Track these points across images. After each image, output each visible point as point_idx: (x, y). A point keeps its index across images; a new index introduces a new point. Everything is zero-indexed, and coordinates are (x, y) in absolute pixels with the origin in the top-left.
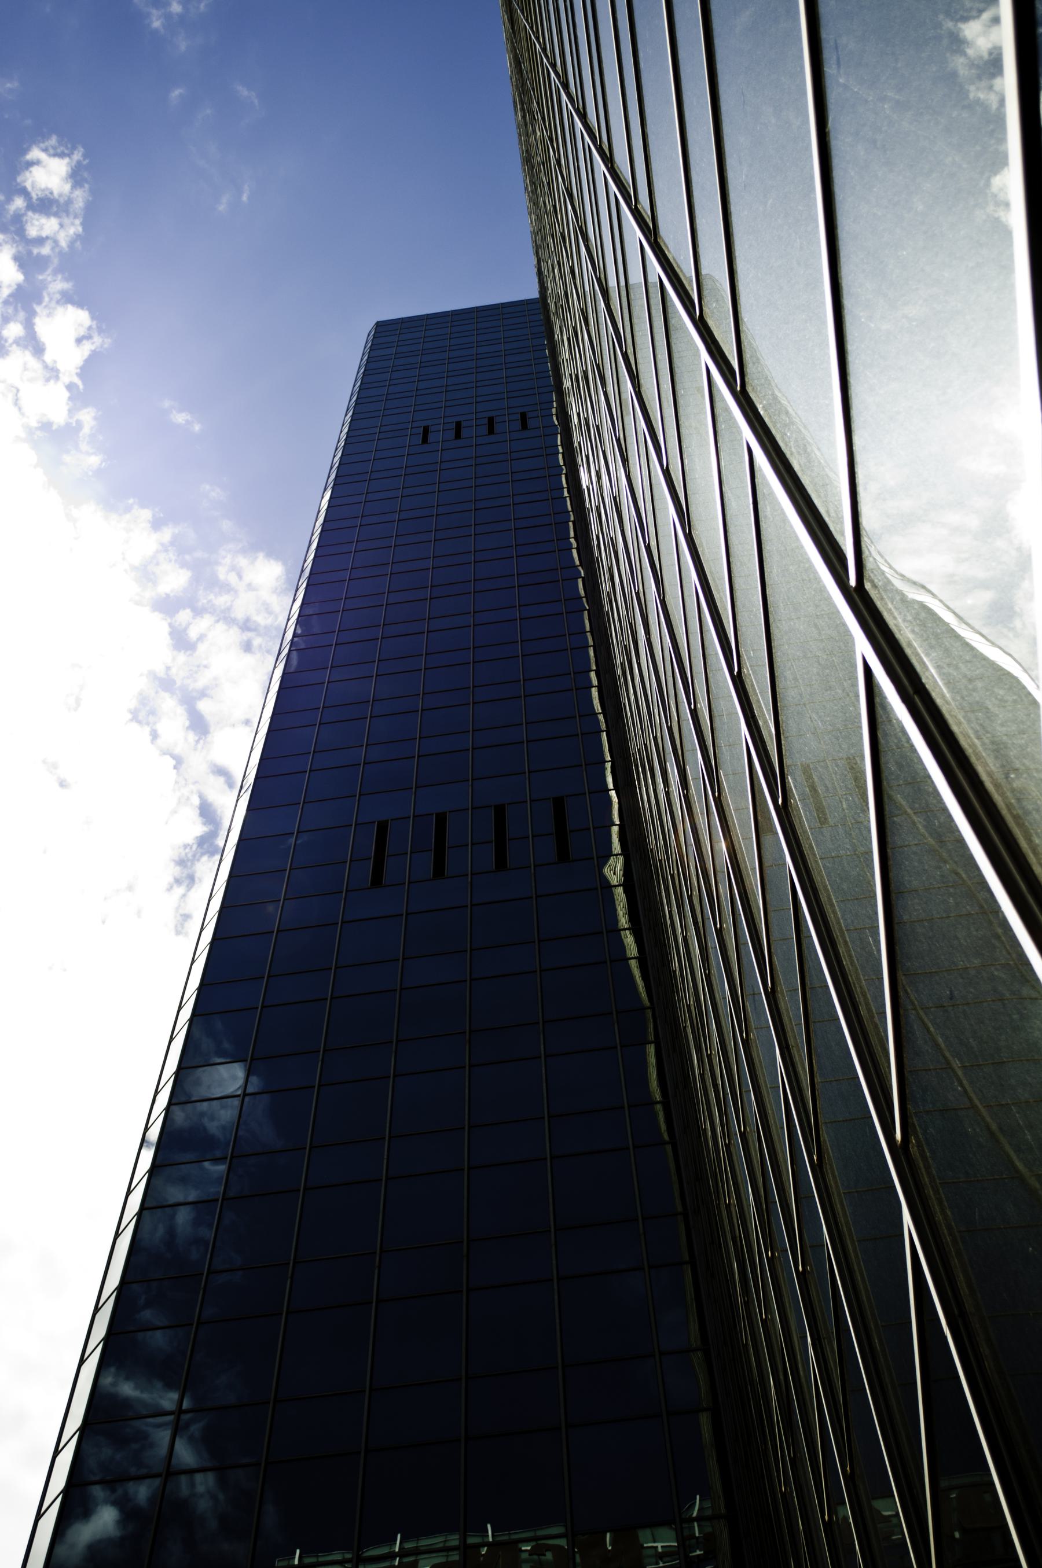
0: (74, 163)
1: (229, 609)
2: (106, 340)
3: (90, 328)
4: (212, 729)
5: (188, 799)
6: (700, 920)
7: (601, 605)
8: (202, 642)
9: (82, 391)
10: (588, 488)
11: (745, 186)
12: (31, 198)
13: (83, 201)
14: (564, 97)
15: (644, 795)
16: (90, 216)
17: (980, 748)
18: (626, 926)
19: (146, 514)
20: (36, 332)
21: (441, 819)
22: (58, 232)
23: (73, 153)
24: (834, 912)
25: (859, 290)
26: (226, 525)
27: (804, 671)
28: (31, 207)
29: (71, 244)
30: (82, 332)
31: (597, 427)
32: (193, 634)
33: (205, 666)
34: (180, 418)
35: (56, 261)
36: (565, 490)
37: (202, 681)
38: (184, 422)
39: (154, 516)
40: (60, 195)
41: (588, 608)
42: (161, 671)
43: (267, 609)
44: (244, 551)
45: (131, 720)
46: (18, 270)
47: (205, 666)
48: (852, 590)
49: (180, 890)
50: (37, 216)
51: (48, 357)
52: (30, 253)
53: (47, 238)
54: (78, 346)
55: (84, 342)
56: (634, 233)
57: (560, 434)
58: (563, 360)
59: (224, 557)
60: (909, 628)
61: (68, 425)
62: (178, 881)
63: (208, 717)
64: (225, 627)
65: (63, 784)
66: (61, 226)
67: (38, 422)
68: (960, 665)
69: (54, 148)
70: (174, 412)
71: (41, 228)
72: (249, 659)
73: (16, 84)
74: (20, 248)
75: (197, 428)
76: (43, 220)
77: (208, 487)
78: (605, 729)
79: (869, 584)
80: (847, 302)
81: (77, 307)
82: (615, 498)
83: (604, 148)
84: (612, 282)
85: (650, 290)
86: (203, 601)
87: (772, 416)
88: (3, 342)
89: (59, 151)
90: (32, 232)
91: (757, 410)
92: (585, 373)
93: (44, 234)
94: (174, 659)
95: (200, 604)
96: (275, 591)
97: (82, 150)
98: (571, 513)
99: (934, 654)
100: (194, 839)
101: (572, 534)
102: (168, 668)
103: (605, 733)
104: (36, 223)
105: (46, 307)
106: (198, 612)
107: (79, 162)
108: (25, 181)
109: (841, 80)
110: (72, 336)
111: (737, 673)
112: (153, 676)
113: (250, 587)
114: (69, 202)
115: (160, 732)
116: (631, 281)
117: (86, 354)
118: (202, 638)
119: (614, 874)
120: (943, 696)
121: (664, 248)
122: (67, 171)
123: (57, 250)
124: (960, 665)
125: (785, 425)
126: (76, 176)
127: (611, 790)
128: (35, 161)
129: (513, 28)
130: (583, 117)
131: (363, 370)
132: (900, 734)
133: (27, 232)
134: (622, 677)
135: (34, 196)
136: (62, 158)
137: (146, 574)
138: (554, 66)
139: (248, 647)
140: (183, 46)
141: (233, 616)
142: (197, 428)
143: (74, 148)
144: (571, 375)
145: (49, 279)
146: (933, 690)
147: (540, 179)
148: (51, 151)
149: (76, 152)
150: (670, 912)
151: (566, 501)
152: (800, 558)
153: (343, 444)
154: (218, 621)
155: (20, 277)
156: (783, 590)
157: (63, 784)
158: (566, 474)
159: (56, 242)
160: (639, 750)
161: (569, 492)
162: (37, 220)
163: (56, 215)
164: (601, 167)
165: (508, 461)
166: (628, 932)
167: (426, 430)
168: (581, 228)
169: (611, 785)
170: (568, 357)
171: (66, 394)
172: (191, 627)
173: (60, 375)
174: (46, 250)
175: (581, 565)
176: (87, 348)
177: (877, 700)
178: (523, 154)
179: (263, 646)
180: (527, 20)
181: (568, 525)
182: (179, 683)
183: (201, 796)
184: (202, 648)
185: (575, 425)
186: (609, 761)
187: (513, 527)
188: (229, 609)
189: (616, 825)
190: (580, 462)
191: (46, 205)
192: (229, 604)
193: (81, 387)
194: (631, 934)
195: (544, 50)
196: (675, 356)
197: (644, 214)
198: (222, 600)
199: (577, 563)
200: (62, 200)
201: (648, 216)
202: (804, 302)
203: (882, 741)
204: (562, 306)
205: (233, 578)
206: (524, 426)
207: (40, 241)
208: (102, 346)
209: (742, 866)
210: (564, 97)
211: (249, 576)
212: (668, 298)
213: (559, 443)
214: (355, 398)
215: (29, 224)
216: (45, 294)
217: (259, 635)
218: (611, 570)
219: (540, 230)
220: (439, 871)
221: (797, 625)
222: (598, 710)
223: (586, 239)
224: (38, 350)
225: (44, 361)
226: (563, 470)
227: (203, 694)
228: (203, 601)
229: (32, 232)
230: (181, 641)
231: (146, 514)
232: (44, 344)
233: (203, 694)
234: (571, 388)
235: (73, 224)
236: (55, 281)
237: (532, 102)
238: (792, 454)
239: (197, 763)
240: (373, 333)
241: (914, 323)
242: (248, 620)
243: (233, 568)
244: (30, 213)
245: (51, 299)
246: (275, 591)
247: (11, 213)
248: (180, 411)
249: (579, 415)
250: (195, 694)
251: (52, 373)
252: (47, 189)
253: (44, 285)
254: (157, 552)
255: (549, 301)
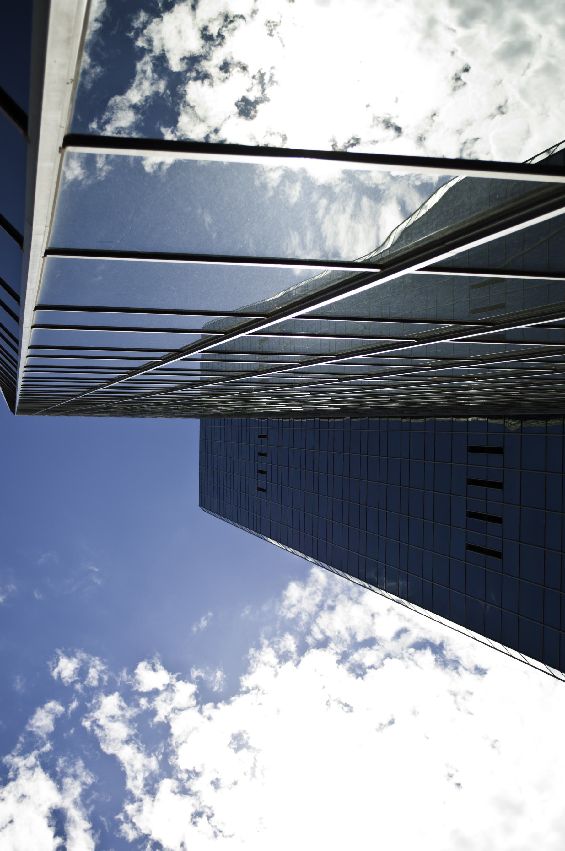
0: (62, 654)
1: (310, 615)
2: (157, 655)
3: (148, 663)
4: (374, 635)
5: (410, 654)
6: (547, 381)
7: (366, 410)
8: (326, 632)
9: (182, 673)
10: (303, 408)
11: (162, 300)
12: (78, 680)
13: (83, 653)
14: (101, 389)
15: (473, 402)
16: (92, 652)
17: (480, 213)
18: (545, 423)
19: (252, 651)
20: (147, 692)
21: (470, 515)
22: (97, 669)
23: (58, 654)
24: (556, 305)
25: (226, 246)
26: (265, 608)
27: (421, 304)
28: (82, 681)
29: (104, 663)
30: (149, 667)
31: (272, 398)
32: (320, 636)
33: (339, 633)
34: (204, 623)
35: (112, 674)
36: (302, 420)
37: (346, 636)
38: (206, 621)
39: (254, 647)
40: (78, 664)
41: (367, 418)
42: (336, 658)
43: (313, 594)
44: (281, 601)
45: (363, 679)
46: (113, 695)
47: (339, 633)
48: (382, 271)
49: (461, 669)
50: (88, 680)
51: (161, 688)
52: (105, 686)
53: (99, 676)
54: (157, 671)
55: (155, 667)
56: (176, 362)
57: (272, 418)
58: (234, 411)
59: (283, 612)
60: (408, 243)
61: (198, 684)
62: (456, 668)
63: (367, 637)
64: (319, 618)
65: (392, 722)
66: (94, 667)
67: (194, 700)
68: (432, 217)
69: (54, 664)
70: (199, 625)
71: (93, 677)
72: (339, 608)
73: (18, 677)
74: (102, 691)
75: (210, 614)
76: (90, 676)
77: (242, 614)
78: (434, 418)
79: (381, 262)
80: (232, 253)
81: (137, 668)
82: (311, 394)
83: (130, 372)
84: (198, 378)
85: (206, 358)
86: (303, 629)
87: (283, 302)
88: (149, 711)
89: (55, 661)
90: (95, 683)
91: (278, 310)
92: (243, 400)
93: (97, 677)
94: (332, 649)
95: (305, 631)
96: (304, 588)
97: (56, 649)
98: (315, 419)
99: (424, 232)
100: (433, 655)
101: (326, 420)
102: (337, 653)
103: (436, 419)
104: (91, 679)
105: (135, 685)
106: (309, 632)
107: (63, 652)
108: (68, 682)
109: (118, 242)
110: (152, 673)
111: (416, 341)
112: (339, 662)
113: (299, 601)
114: (82, 660)
115: (370, 665)
116: (199, 368)
117: (162, 668)
118: (322, 632)
119: (514, 425)
120: (448, 229)
121: (186, 348)
122: (66, 658)
123: (106, 672)
124: (432, 217)
125: (289, 295)
126: (70, 655)
127: (468, 420)
128: (58, 675)
129: (62, 411)
130: (113, 380)
131: (223, 517)
132: (464, 255)
133: (95, 686)
134: (408, 405)
135: (77, 678)
136: (59, 660)
137: (283, 658)
138: (84, 392)
139: (332, 608)
140: (14, 587)
141: (313, 613)
142: (210, 614)
143: (56, 653)
144: (243, 408)
145: (120, 679)
146: (444, 234)
147: (139, 408)
148: (55, 665)
149: (57, 652)
150: (541, 397)
151: (308, 421)
152: (360, 297)
153: (260, 534)
154: (315, 621)
155: (117, 694)
156: (376, 309)
157: (392, 722)
158: (294, 418)
159: (102, 672)
160: (448, 401)
161: (304, 419)
162: (90, 679)
163: (88, 669)
164: (139, 375)
165: (334, 453)
166: (548, 422)
167: (259, 489)
168: (168, 391)
169: (465, 419)
170: (233, 408)
171: (181, 682)
172: (316, 637)
173: (172, 683)
174: (106, 678)
175: (343, 418)
176: (158, 666)
177: (444, 265)
178: (125, 416)
179: (333, 599)
180: (59, 403)
181: (321, 421)
182: (346, 649)
183: (410, 647)
184: (329, 633)
185: (269, 409)
186: (452, 419)
187: (450, 464)
188: (310, 615)
189: (488, 420)
190: (289, 410)
191: (82, 672)
192: (307, 614)
193: (180, 673)
194: (549, 421)
195: (75, 396)
196: (244, 350)
197: (169, 355)
198: (304, 617)
199: (342, 420)
200: (81, 664)
201: (169, 354)
202: (227, 277)
203: (466, 266)
204: (206, 407)
205: (294, 610)
206: (265, 437)
207: (100, 680)
208: (159, 659)
209: (522, 353)
210: (101, 389)
211: (294, 601)
212: (212, 349)
213: (277, 420)
214: (237, 524)
215: (91, 684)
216: (127, 683)
217: (326, 601)
218: (349, 402)
219: (166, 412)
220: (498, 520)
221: (396, 304)
222: (423, 420)
223: (175, 389)
224: (155, 692)
225: (163, 691)
226: (291, 420)
227: (353, 637)
228: (303, 629)
229: (95, 683)
230: (323, 644)
231: (252, 651)
232: (153, 689)
233: (353, 637)
234: (250, 409)
235: (94, 661)
236: (122, 677)
237: (100, 407)
238: (305, 294)
239: (391, 646)
240: (204, 509)
241: (248, 219)
242: (317, 605)
243: (289, 609)
244: (85, 683)
245: (130, 680)
246: (304, 588)
247: (83, 692)
248: (200, 622)
249: (264, 407)
250: (353, 642)
251: (169, 687)
252: (74, 671)
253: (122, 683)
254: (272, 648)
255: (202, 414)
